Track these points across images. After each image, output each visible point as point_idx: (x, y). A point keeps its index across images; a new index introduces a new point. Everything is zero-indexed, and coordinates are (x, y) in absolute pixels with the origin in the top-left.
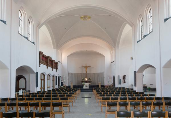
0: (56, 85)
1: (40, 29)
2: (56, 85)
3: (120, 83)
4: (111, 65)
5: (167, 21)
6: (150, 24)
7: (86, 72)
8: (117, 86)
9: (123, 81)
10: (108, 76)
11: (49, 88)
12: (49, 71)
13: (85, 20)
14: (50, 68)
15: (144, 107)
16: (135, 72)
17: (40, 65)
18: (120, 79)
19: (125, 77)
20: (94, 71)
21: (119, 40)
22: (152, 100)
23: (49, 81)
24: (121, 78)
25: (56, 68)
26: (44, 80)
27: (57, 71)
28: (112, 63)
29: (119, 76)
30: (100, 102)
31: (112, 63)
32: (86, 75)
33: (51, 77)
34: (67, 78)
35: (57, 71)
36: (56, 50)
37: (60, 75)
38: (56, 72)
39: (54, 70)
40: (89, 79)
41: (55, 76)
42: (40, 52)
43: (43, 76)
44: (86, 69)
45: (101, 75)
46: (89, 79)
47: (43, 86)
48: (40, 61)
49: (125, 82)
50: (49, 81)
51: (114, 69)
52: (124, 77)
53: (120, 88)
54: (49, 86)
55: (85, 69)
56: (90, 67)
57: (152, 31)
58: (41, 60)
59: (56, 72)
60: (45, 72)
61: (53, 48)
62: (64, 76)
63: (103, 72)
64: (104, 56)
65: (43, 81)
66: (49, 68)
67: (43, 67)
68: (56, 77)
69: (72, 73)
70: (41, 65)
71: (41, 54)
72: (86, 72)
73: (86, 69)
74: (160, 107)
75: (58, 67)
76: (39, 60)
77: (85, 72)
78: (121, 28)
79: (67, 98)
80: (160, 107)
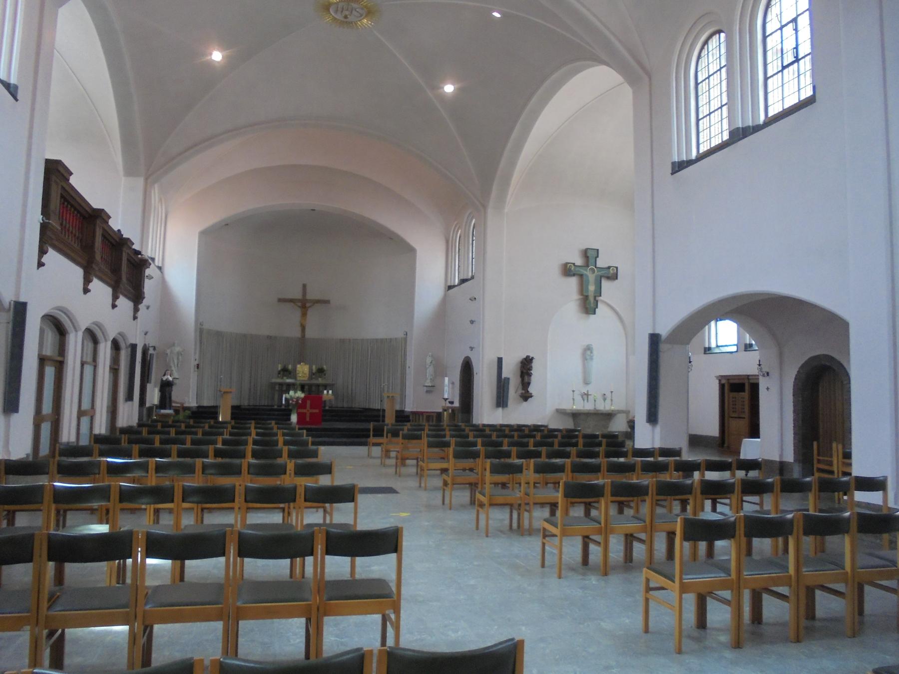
0: (129, 397)
1: (61, 6)
2: (129, 397)
3: (501, 401)
4: (444, 301)
5: (157, 270)
6: (789, 58)
7: (303, 328)
8: (486, 414)
9: (520, 391)
10: (429, 360)
11: (592, 558)
12: (95, 305)
13: (346, 23)
14: (100, 289)
15: (641, 541)
16: (654, 340)
17: (42, 252)
18: (503, 376)
19: (530, 369)
20: (341, 328)
21: (512, 164)
22: (559, 475)
23: (88, 369)
24: (510, 370)
25: (137, 297)
26: (60, 366)
27: (136, 310)
28: (450, 287)
29: (500, 360)
30: (806, 628)
31: (450, 287)
32: (302, 348)
33: (105, 351)
34: (193, 363)
35: (136, 310)
36: (140, 182)
37: (151, 341)
38: (135, 318)
39: (124, 303)
40: (321, 371)
41: (122, 345)
42: (48, 161)
43: (51, 336)
44: (304, 315)
45: (390, 352)
46: (321, 371)
47: (47, 408)
48: (44, 228)
49: (526, 396)
50: (88, 369)
51: (472, 322)
52: (526, 366)
53: (501, 430)
54: (86, 406)
55: (298, 313)
56: (327, 302)
57: (810, 101)
58: (54, 223)
59: (135, 318)
60: (64, 305)
61: (121, 172)
62: (177, 349)
63: (400, 335)
64: (412, 250)
65: (50, 371)
66: (96, 285)
67: (62, 271)
68: (134, 347)
69: (219, 334)
70: (52, 256)
71: (54, 178)
72: (303, 328)
73: (304, 315)
74: (588, 508)
75: (149, 287)
76: (39, 218)
77: (297, 333)
78: (534, 100)
79: (148, 462)
80: (588, 508)
